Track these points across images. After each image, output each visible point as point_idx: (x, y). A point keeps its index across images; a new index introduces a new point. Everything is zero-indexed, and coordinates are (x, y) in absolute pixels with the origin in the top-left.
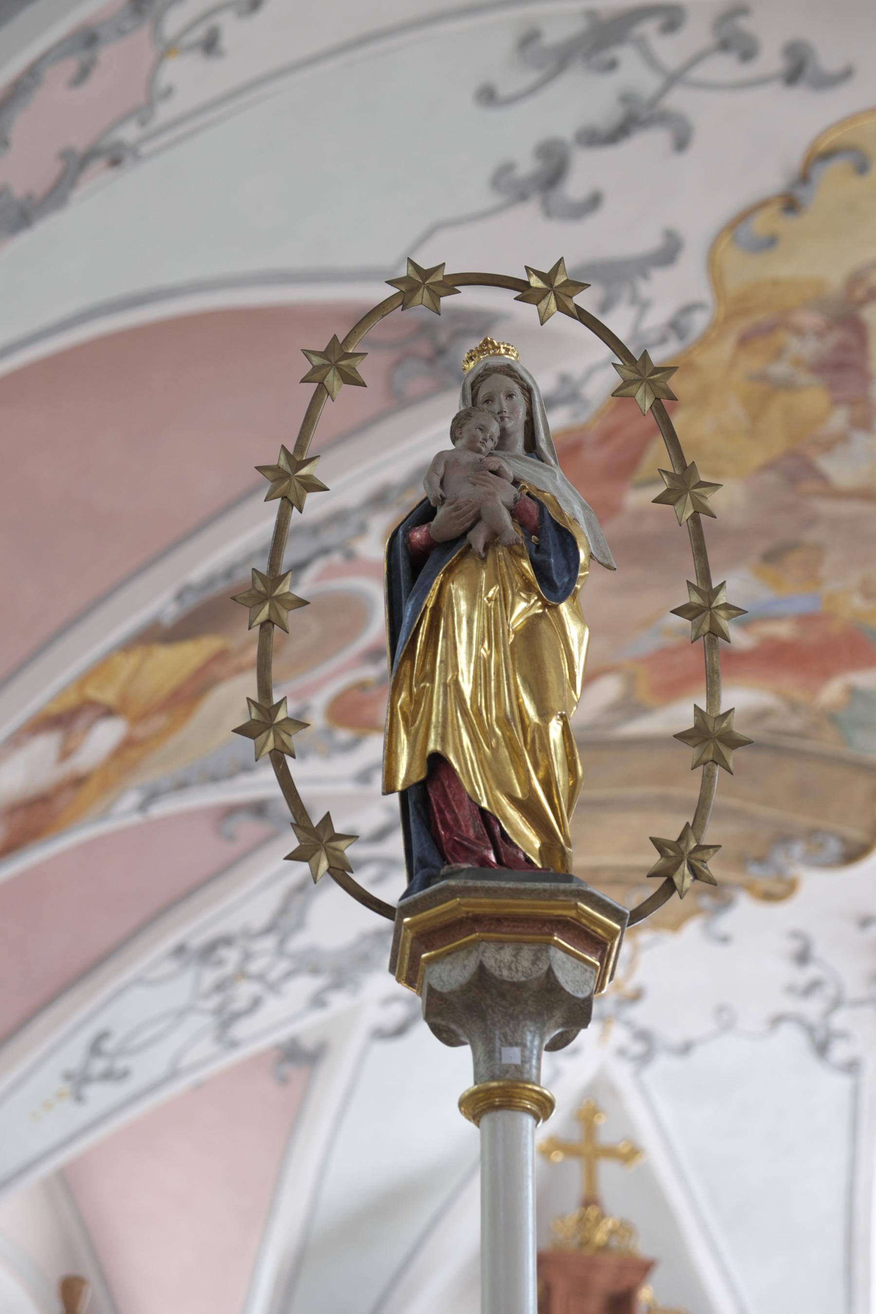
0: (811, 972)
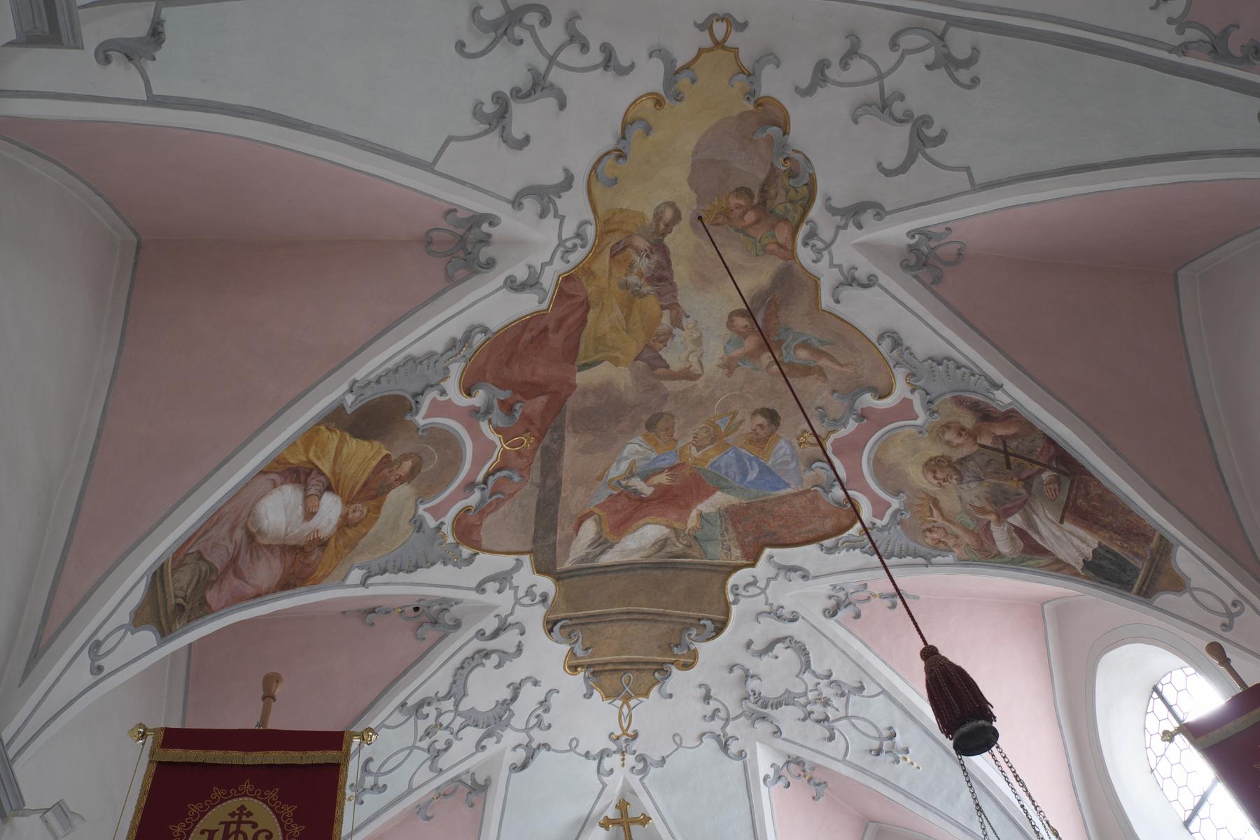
0: (713, 704)
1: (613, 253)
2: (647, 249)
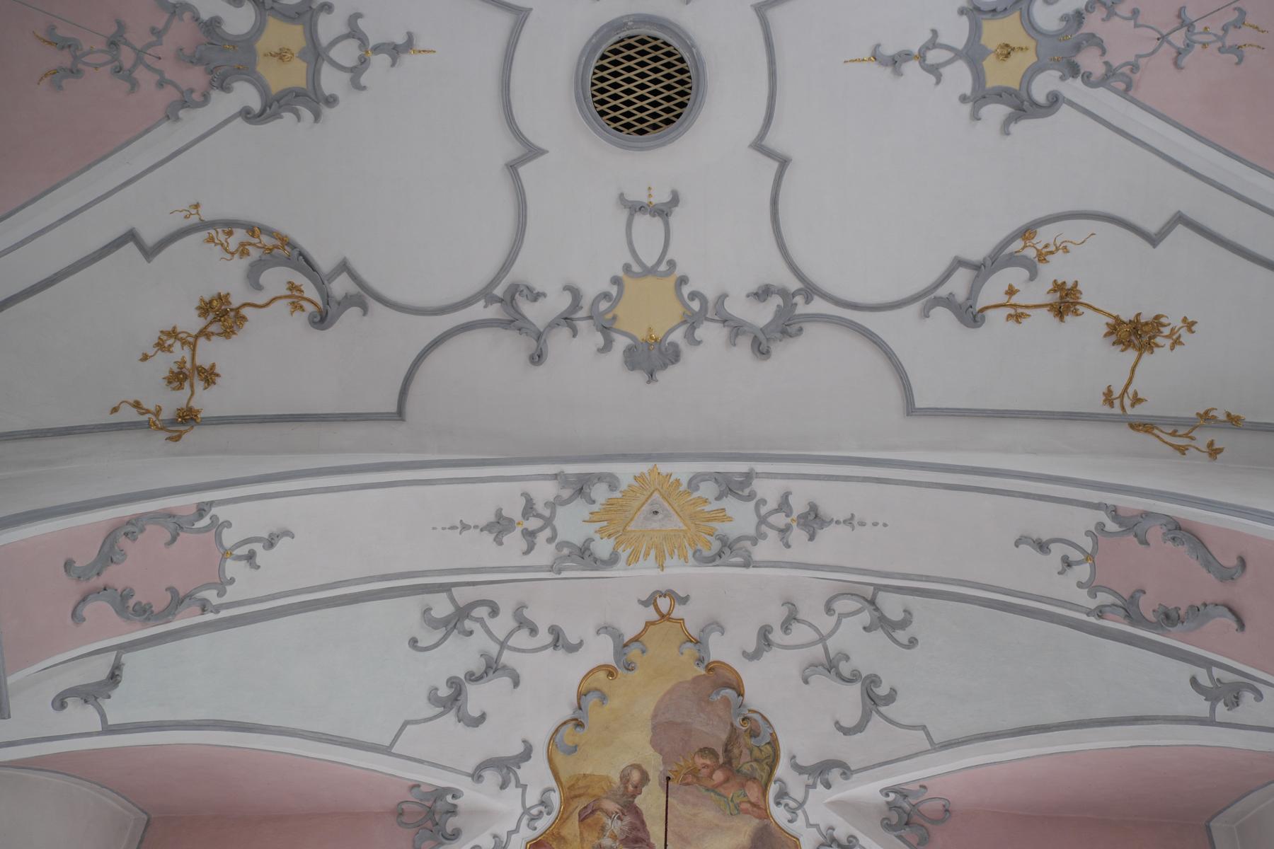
1: (582, 818)
2: (618, 811)
